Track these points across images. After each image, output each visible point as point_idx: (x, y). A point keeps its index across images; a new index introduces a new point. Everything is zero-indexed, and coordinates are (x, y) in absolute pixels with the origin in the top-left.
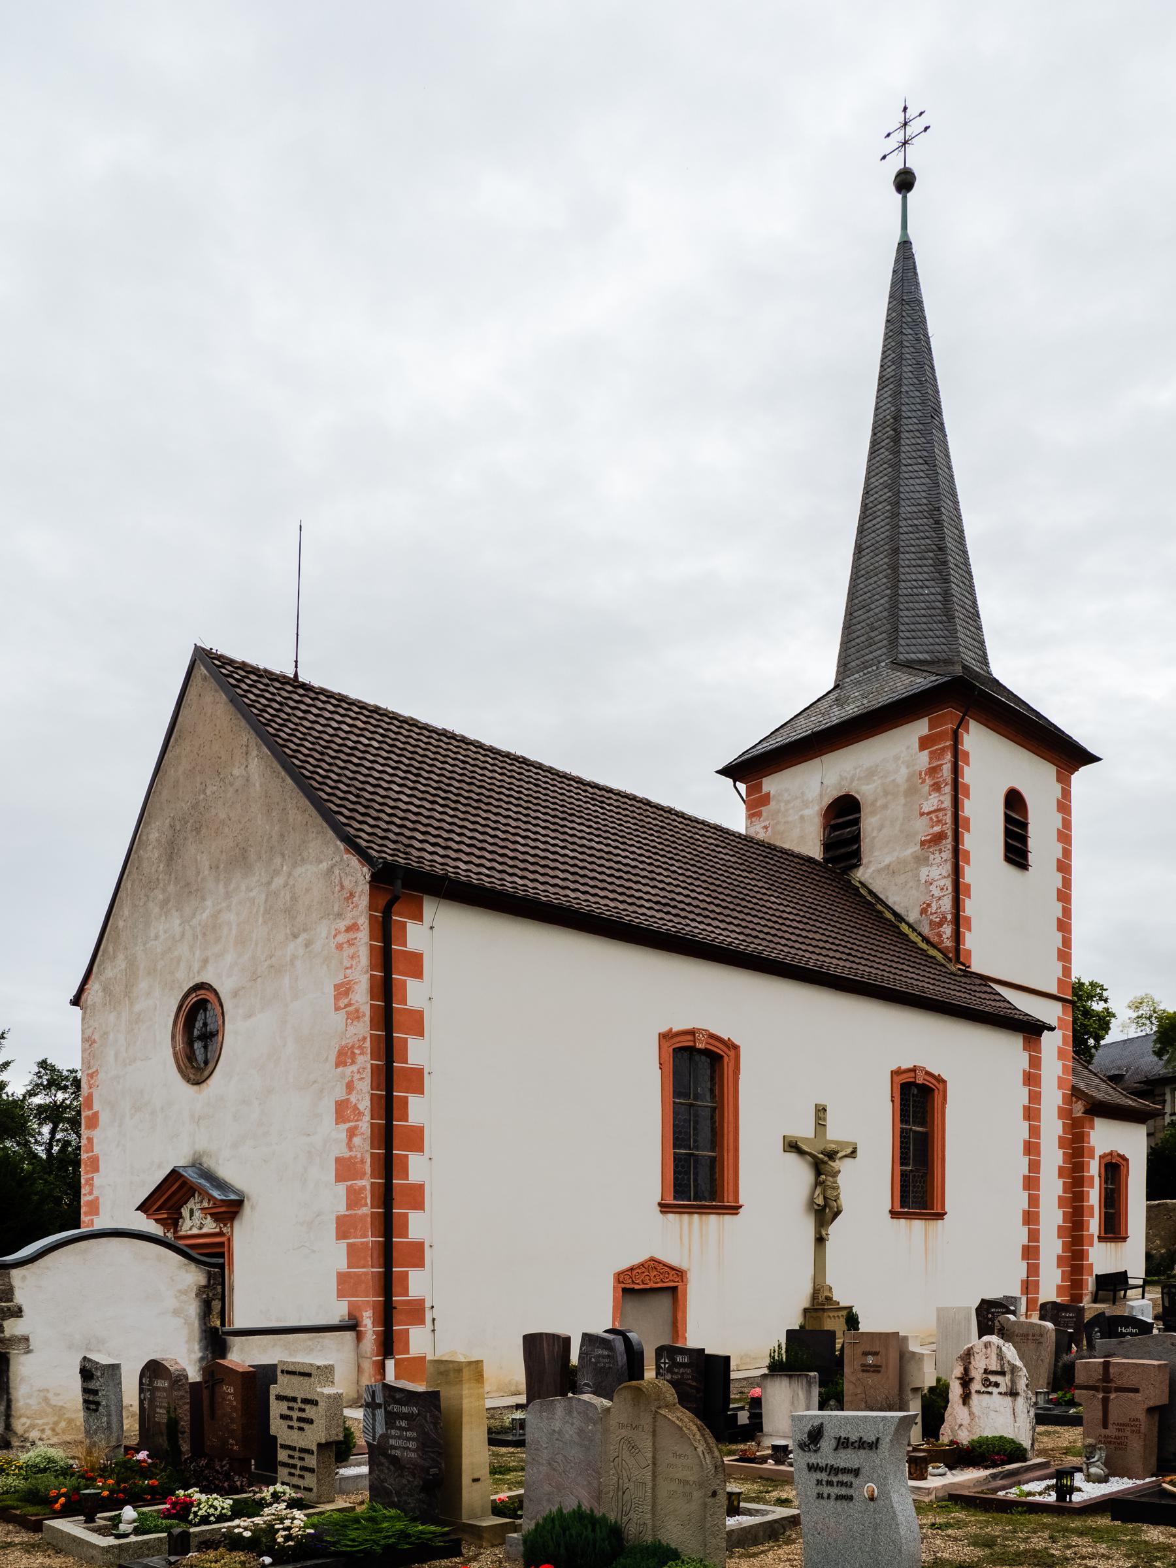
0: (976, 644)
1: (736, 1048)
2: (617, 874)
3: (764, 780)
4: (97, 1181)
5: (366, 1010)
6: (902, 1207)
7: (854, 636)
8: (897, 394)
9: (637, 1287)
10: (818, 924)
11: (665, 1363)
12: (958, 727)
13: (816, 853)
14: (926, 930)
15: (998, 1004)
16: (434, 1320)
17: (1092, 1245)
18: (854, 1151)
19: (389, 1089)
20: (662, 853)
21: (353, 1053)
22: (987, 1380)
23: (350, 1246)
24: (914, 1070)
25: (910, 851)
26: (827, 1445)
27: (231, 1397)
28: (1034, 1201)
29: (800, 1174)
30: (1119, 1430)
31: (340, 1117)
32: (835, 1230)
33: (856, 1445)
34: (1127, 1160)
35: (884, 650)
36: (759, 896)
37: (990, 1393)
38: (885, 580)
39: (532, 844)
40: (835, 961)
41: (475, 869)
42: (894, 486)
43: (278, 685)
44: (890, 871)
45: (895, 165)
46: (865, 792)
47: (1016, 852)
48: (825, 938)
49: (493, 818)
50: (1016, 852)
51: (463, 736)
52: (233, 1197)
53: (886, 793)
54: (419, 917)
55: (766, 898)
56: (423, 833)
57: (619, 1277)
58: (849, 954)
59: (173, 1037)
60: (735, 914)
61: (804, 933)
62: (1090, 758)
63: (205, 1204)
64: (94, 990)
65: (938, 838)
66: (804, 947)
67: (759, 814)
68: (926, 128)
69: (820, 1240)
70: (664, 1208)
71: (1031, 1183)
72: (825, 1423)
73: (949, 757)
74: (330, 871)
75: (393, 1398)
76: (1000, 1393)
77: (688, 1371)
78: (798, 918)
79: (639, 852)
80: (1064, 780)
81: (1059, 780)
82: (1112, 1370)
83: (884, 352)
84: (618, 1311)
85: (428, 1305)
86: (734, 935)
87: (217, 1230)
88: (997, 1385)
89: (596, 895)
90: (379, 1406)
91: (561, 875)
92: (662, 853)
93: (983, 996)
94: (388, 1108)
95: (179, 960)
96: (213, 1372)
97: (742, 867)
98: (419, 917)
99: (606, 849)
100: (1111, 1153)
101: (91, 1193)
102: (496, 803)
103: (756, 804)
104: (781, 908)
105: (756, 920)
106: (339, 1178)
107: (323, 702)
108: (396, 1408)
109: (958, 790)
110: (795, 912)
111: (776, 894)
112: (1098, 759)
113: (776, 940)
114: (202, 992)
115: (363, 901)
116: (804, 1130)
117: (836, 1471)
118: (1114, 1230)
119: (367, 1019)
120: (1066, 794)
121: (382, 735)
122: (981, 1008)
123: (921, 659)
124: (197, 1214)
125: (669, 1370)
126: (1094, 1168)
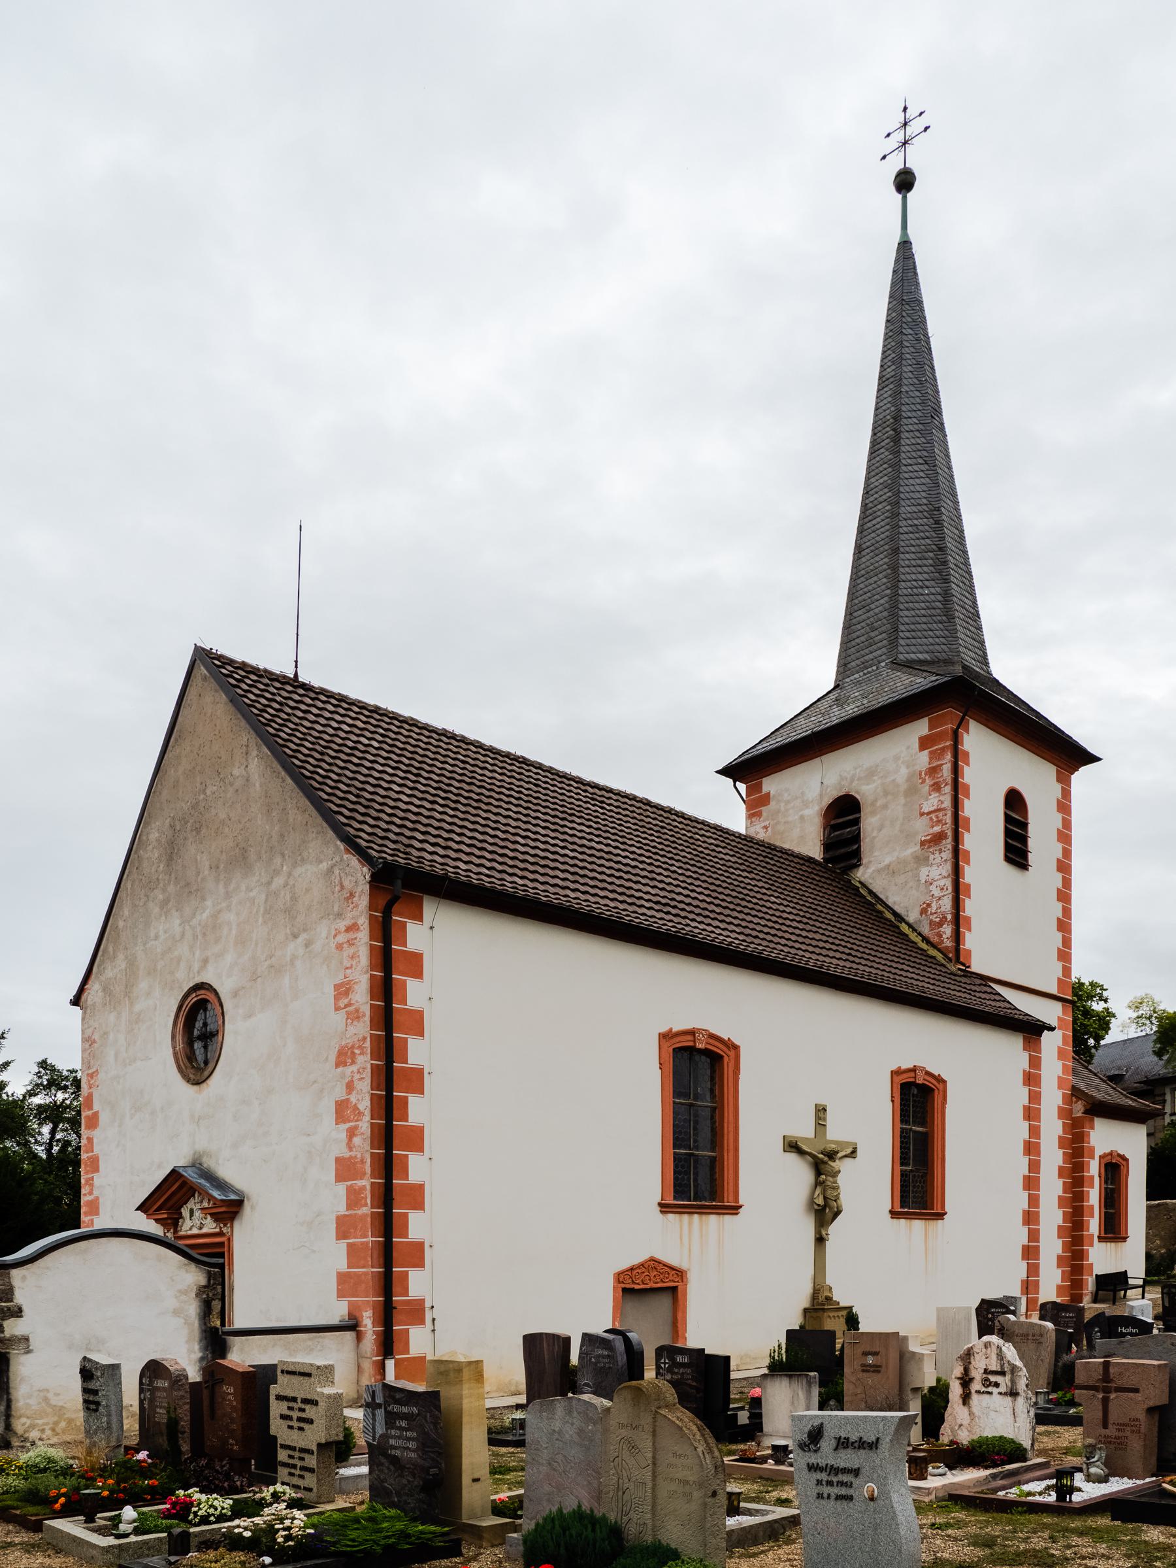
0: (976, 644)
1: (736, 1048)
2: (617, 874)
3: (764, 780)
4: (97, 1181)
5: (366, 1010)
6: (902, 1207)
7: (854, 636)
8: (897, 394)
9: (637, 1287)
10: (818, 924)
11: (665, 1363)
12: (958, 727)
13: (816, 853)
14: (926, 930)
15: (998, 1004)
16: (434, 1320)
17: (1092, 1245)
18: (854, 1151)
19: (389, 1089)
20: (662, 853)
21: (353, 1053)
22: (987, 1380)
23: (350, 1246)
24: (914, 1070)
25: (910, 851)
26: (827, 1445)
27: (231, 1397)
28: (1034, 1201)
29: (800, 1174)
30: (1119, 1430)
31: (340, 1117)
32: (835, 1230)
33: (856, 1445)
34: (1127, 1160)
35: (884, 650)
36: (759, 896)
37: (990, 1393)
38: (885, 580)
39: (532, 844)
40: (835, 961)
41: (475, 869)
42: (894, 486)
43: (278, 685)
44: (890, 871)
45: (895, 165)
46: (865, 792)
47: (1016, 852)
48: (825, 938)
49: (493, 818)
50: (1016, 852)
51: (463, 736)
52: (233, 1197)
53: (886, 793)
54: (419, 917)
55: (766, 898)
56: (423, 833)
57: (619, 1277)
58: (849, 954)
59: (173, 1037)
60: (735, 914)
61: (804, 933)
62: (1090, 758)
63: (205, 1204)
64: (94, 990)
65: (938, 838)
66: (804, 947)
67: (759, 814)
68: (926, 128)
69: (820, 1240)
70: (664, 1208)
71: (1031, 1183)
72: (825, 1423)
73: (949, 757)
74: (330, 871)
75: (393, 1398)
76: (1000, 1393)
77: (688, 1371)
78: (798, 918)
79: (639, 852)
80: (1064, 780)
81: (1059, 780)
82: (1112, 1370)
83: (884, 352)
84: (618, 1311)
85: (428, 1305)
86: (734, 935)
87: (217, 1230)
88: (997, 1385)
89: (596, 895)
90: (379, 1406)
91: (561, 875)
92: (662, 853)
93: (983, 996)
94: (388, 1108)
95: (179, 960)
96: (213, 1372)
97: (742, 867)
98: (419, 917)
99: (606, 849)
100: (1111, 1153)
101: (91, 1193)
102: (496, 803)
103: (756, 804)
104: (781, 908)
105: (756, 920)
106: (339, 1178)
107: (323, 702)
108: (396, 1408)
109: (958, 790)
110: (795, 912)
111: (776, 894)
112: (1098, 759)
113: (776, 940)
114: (202, 992)
115: (363, 901)
116: (804, 1130)
117: (836, 1471)
118: (1114, 1230)
119: (367, 1019)
120: (1066, 794)
121: (382, 735)
122: (981, 1008)
123: (921, 659)
124: (197, 1214)
125: (669, 1370)
126: (1094, 1168)
